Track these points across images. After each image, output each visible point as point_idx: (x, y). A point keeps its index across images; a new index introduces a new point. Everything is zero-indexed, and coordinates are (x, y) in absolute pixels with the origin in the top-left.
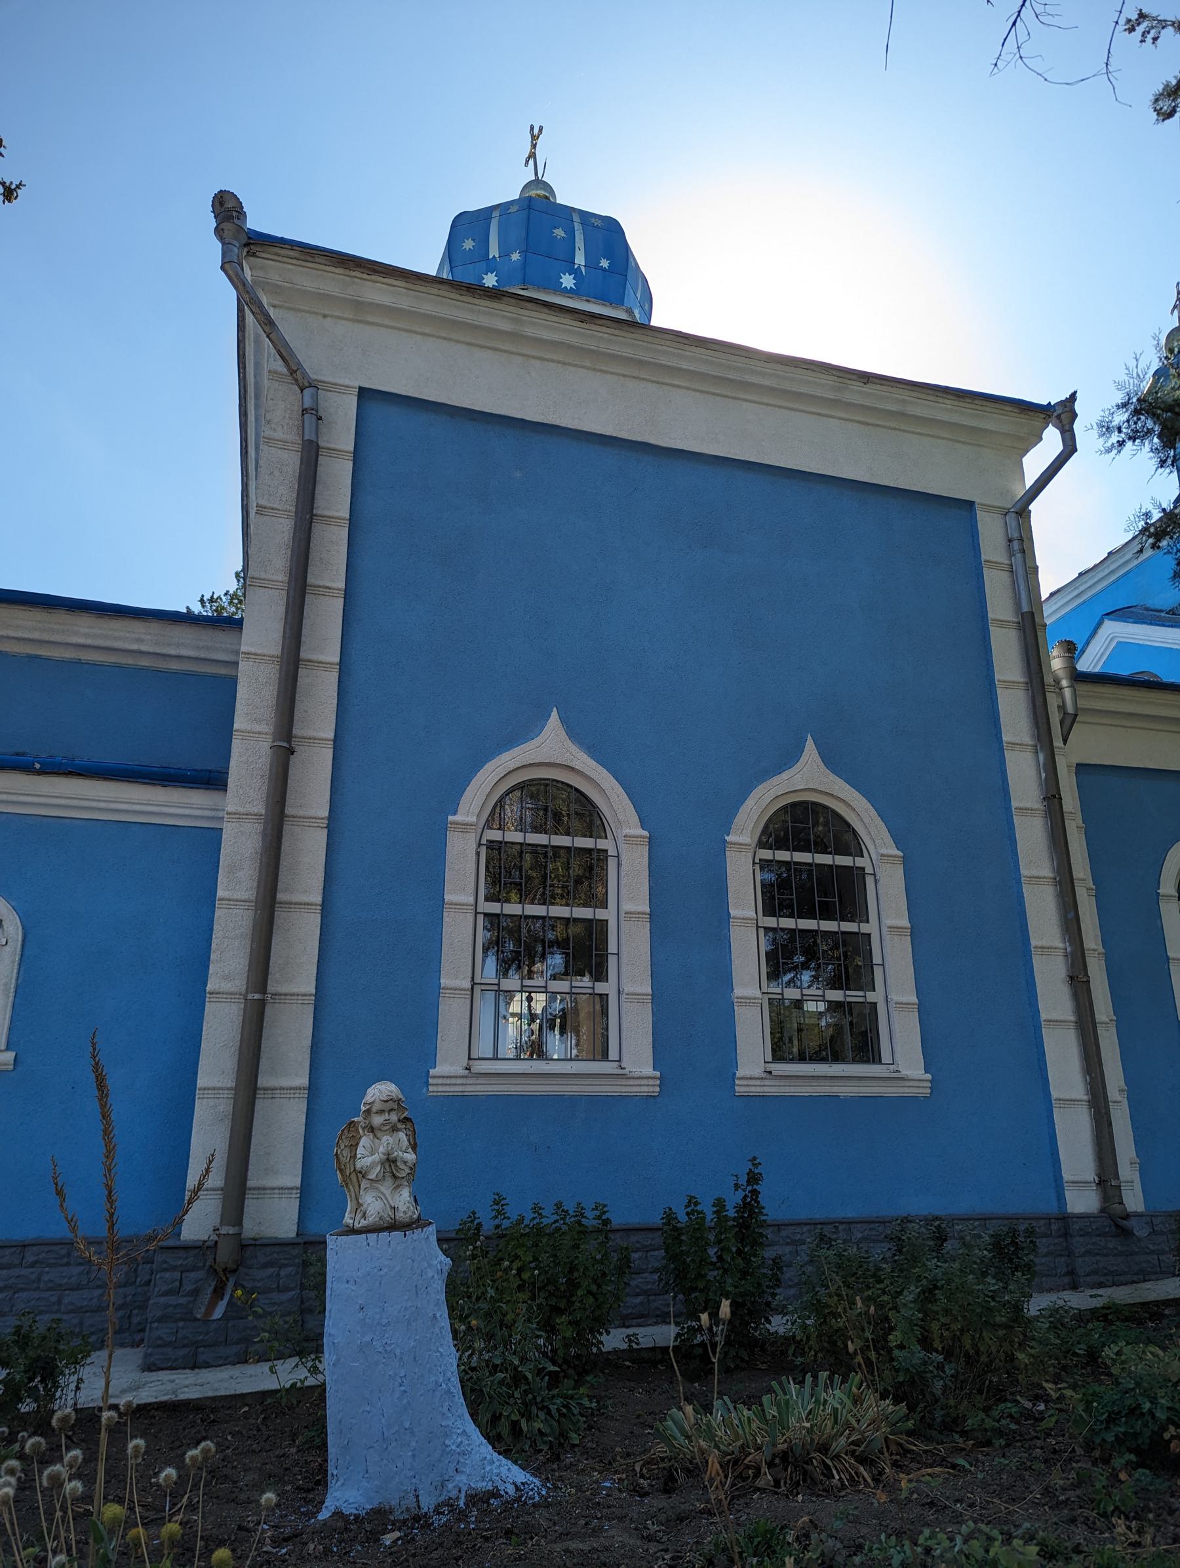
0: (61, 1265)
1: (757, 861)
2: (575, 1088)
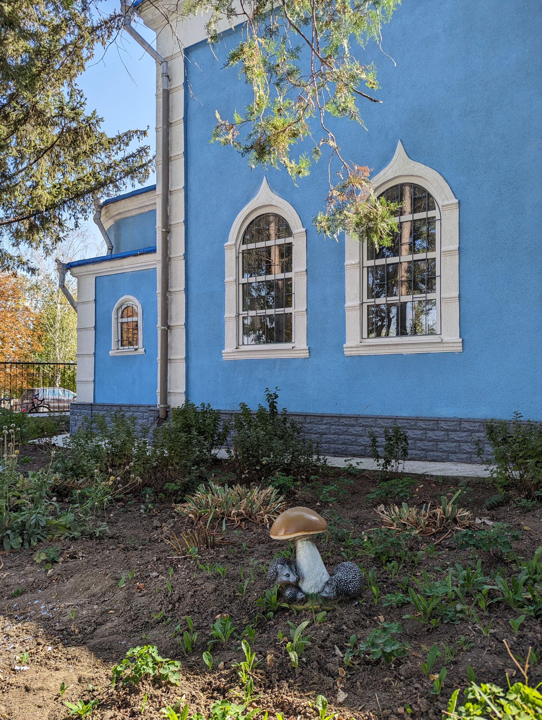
0: (413, 429)
1: (241, 251)
2: (260, 356)
